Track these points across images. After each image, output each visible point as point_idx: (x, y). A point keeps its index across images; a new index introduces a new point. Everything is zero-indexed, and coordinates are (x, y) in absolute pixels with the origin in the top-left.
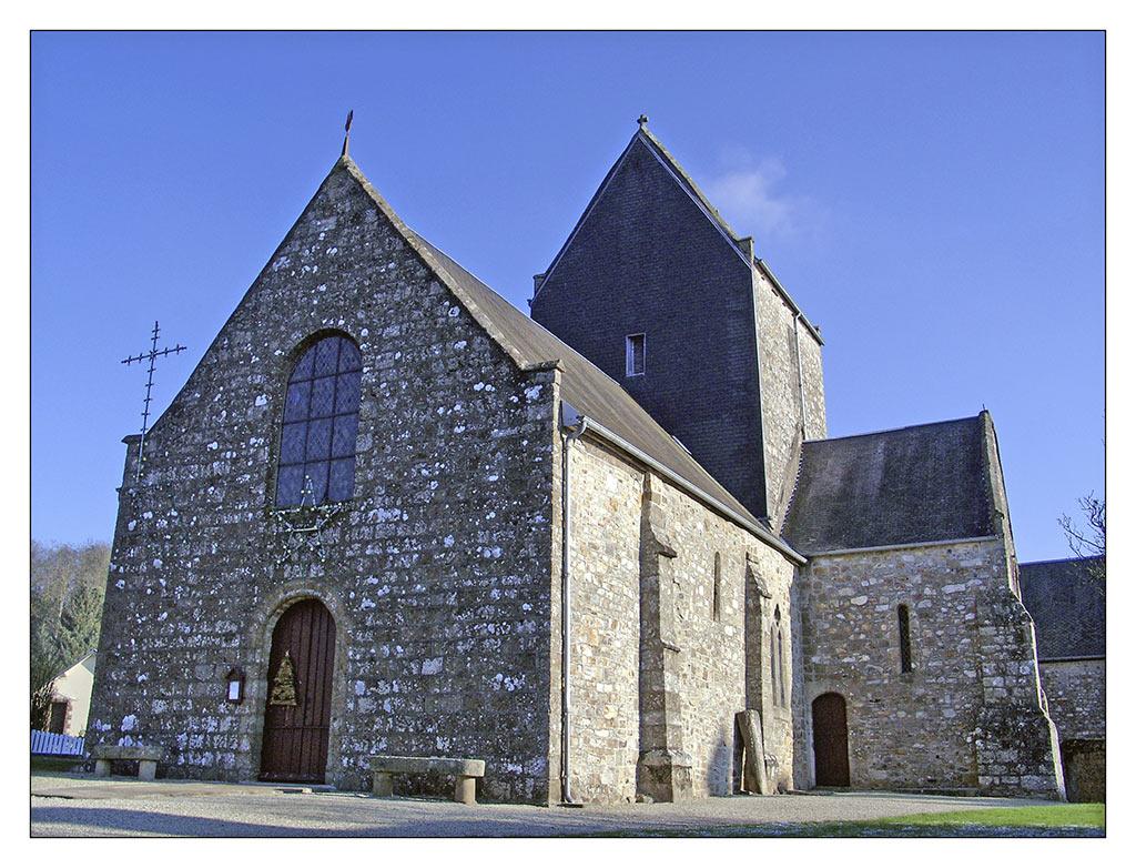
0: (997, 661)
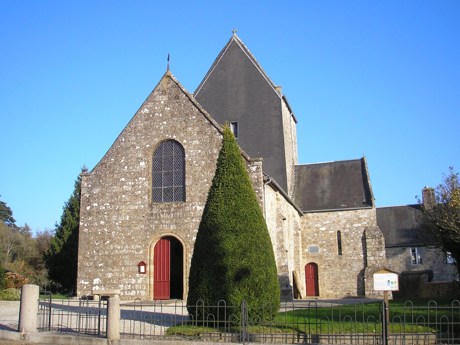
0: (372, 251)
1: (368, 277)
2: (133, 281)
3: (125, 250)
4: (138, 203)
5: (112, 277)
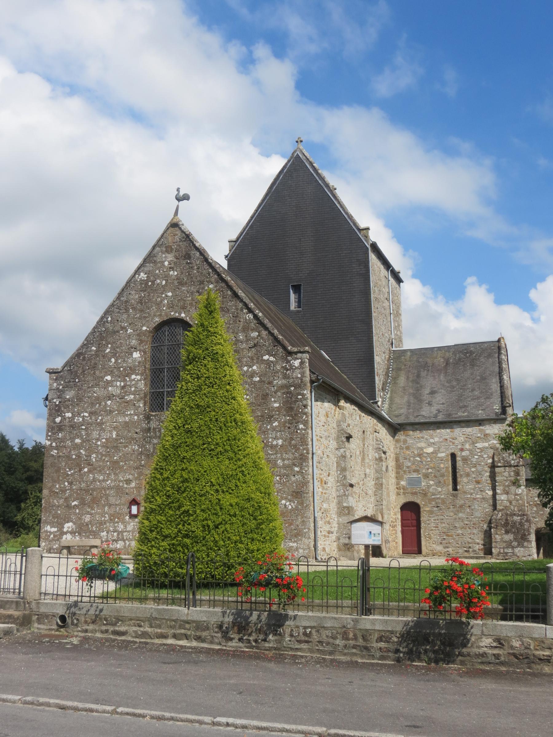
1: (497, 526)
2: (121, 527)
3: (109, 481)
4: (129, 413)
5: (90, 521)
